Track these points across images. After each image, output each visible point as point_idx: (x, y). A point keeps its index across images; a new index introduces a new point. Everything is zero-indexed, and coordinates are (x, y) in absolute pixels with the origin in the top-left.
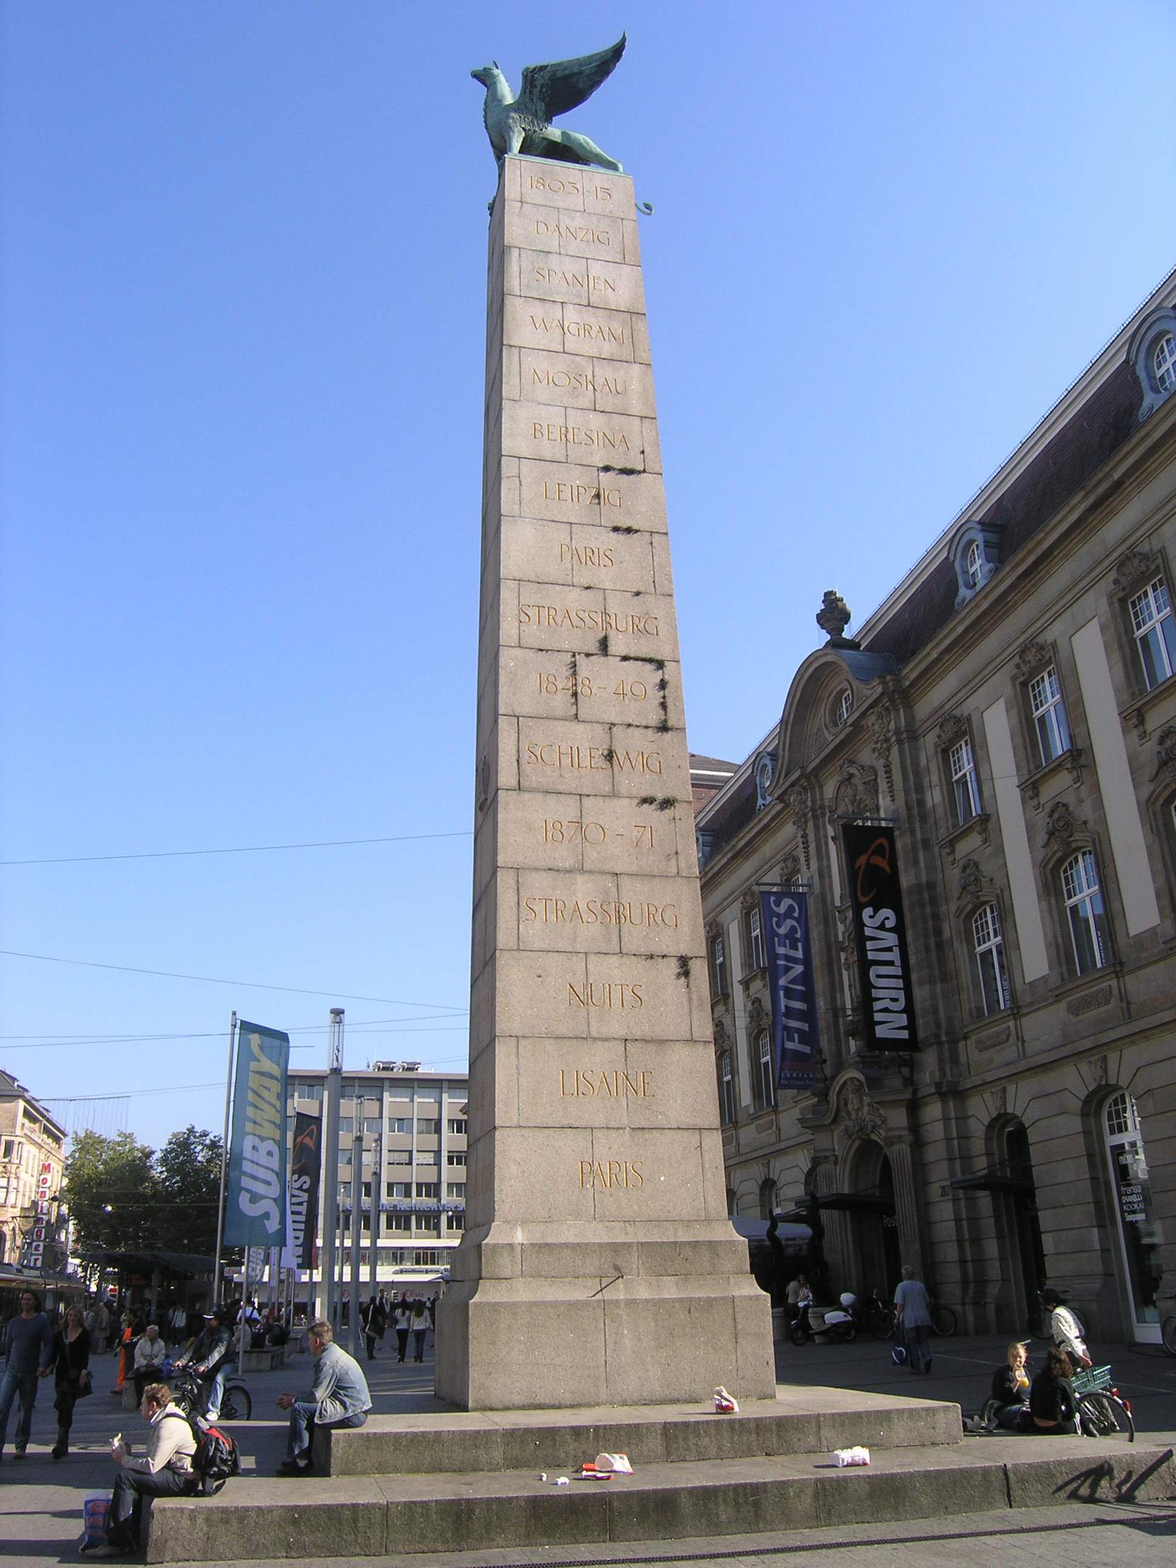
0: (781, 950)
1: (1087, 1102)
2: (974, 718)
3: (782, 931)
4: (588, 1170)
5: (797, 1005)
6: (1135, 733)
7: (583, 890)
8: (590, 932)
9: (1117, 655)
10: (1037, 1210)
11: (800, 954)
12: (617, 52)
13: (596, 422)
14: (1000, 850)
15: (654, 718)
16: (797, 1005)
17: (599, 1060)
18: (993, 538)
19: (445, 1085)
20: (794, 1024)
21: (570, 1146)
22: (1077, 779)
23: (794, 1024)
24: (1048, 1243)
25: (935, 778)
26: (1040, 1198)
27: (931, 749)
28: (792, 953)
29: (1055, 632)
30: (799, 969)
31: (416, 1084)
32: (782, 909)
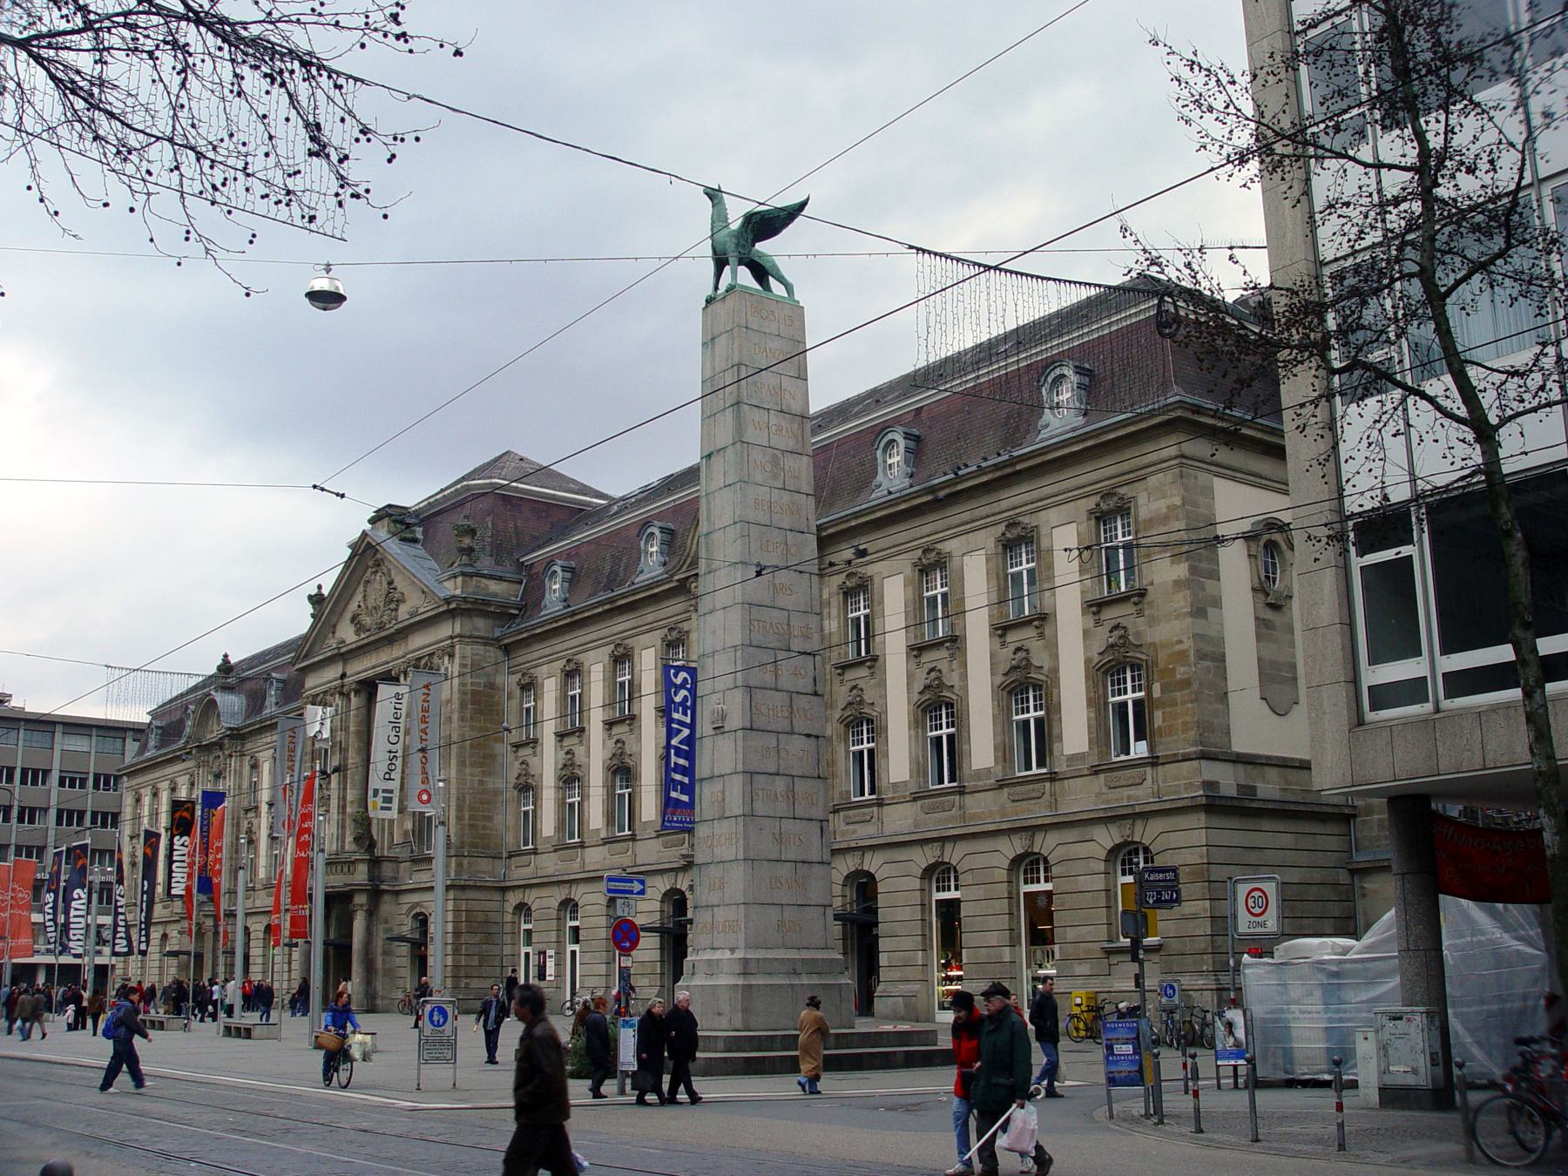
0: (675, 716)
1: (926, 870)
2: (876, 580)
3: (678, 699)
4: (781, 924)
5: (681, 761)
6: (998, 640)
7: (780, 784)
8: (781, 807)
9: (994, 582)
10: (877, 937)
11: (688, 720)
12: (803, 205)
13: (786, 496)
14: (882, 684)
15: (810, 689)
16: (681, 761)
17: (785, 871)
18: (912, 444)
19: (59, 728)
20: (678, 777)
21: (774, 912)
22: (952, 655)
23: (678, 777)
24: (883, 959)
25: (834, 611)
26: (882, 929)
27: (835, 589)
28: (683, 718)
29: (951, 546)
30: (686, 732)
31: (59, 728)
32: (679, 681)
